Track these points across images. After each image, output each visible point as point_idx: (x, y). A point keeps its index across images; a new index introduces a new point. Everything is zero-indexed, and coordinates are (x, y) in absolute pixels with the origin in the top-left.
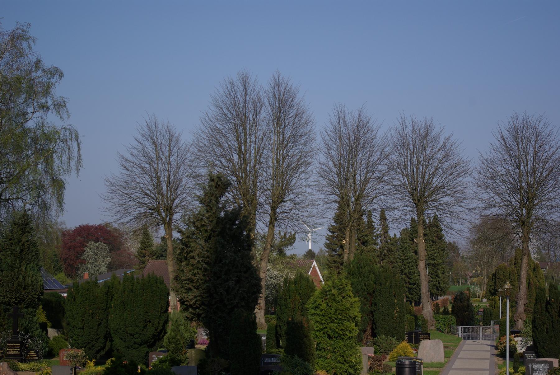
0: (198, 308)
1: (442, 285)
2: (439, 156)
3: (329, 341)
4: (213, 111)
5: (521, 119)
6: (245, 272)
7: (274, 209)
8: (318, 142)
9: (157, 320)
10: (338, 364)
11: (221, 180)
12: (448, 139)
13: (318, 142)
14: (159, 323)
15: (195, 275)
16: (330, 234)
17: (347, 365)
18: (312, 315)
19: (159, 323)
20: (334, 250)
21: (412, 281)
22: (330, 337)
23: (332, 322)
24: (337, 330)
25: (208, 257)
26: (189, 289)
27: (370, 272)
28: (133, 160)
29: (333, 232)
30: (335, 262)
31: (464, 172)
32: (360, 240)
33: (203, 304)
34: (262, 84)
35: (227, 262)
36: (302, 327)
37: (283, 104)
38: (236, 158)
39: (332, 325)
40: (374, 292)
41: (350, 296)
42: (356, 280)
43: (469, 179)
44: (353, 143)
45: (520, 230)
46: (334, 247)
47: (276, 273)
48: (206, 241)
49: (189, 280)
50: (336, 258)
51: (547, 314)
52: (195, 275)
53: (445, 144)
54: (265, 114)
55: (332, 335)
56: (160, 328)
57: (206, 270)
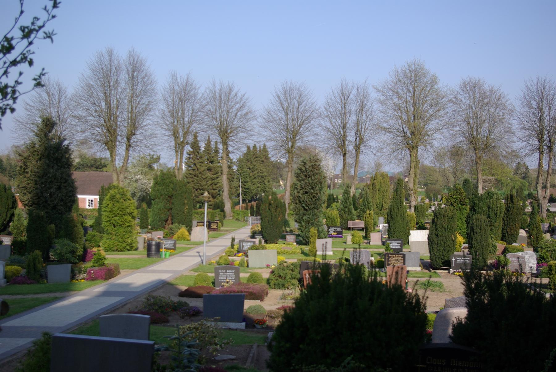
0: (31, 206)
1: (267, 190)
2: (238, 106)
3: (114, 229)
4: (88, 73)
5: (289, 84)
6: (65, 183)
7: (129, 139)
8: (159, 96)
9: (5, 214)
10: (120, 244)
11: (49, 121)
12: (244, 95)
13: (159, 96)
14: (6, 216)
15: (28, 184)
16: (188, 156)
17: (125, 244)
18: (105, 211)
19: (6, 216)
20: (190, 167)
21: (246, 187)
22: (114, 226)
23: (116, 216)
24: (119, 222)
25: (38, 172)
26: (25, 194)
27: (170, 182)
28: (33, 104)
29: (190, 155)
30: (190, 174)
31: (255, 118)
32: (208, 160)
33: (34, 203)
34: (122, 55)
35: (50, 176)
36: (73, 220)
37: (136, 69)
38: (103, 104)
39: (115, 218)
40: (172, 196)
41: (129, 199)
42: (160, 188)
43: (255, 122)
44: (182, 95)
45: (287, 155)
46: (190, 164)
47: (146, 181)
48: (37, 161)
49: (25, 187)
50: (191, 172)
51: (269, 211)
52: (28, 184)
53: (241, 99)
54: (124, 77)
55: (116, 224)
56: (8, 219)
57: (36, 181)
